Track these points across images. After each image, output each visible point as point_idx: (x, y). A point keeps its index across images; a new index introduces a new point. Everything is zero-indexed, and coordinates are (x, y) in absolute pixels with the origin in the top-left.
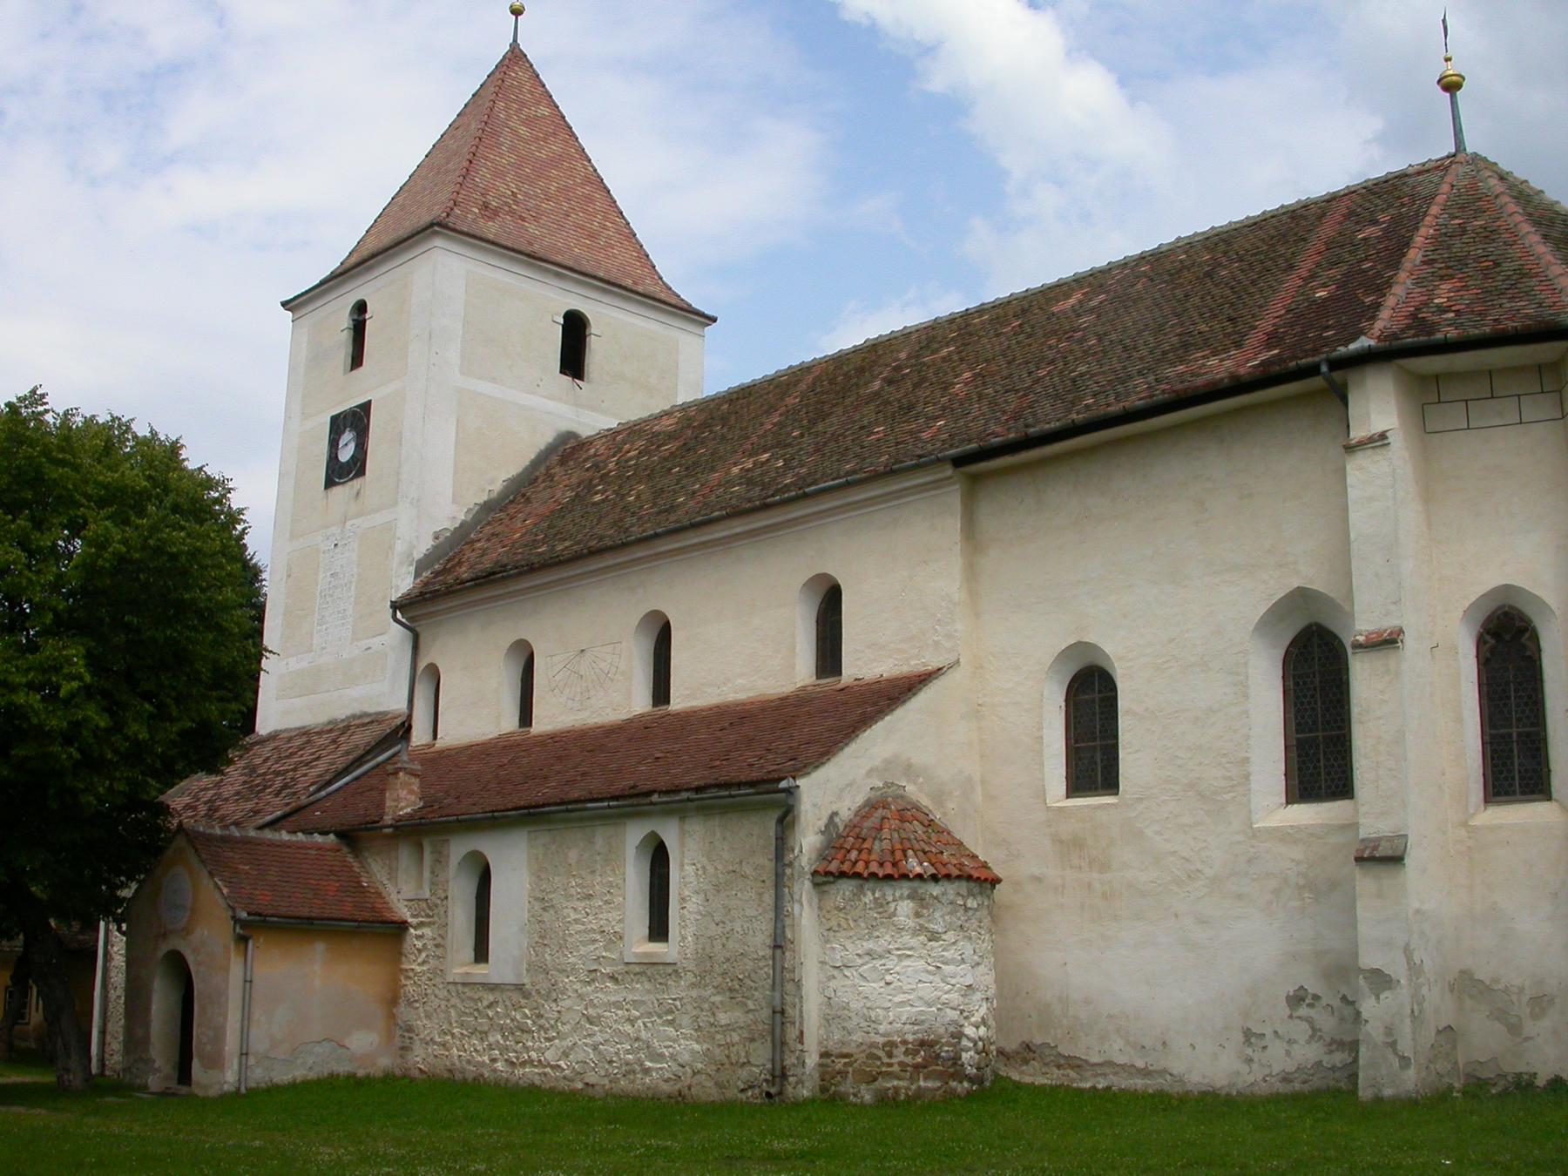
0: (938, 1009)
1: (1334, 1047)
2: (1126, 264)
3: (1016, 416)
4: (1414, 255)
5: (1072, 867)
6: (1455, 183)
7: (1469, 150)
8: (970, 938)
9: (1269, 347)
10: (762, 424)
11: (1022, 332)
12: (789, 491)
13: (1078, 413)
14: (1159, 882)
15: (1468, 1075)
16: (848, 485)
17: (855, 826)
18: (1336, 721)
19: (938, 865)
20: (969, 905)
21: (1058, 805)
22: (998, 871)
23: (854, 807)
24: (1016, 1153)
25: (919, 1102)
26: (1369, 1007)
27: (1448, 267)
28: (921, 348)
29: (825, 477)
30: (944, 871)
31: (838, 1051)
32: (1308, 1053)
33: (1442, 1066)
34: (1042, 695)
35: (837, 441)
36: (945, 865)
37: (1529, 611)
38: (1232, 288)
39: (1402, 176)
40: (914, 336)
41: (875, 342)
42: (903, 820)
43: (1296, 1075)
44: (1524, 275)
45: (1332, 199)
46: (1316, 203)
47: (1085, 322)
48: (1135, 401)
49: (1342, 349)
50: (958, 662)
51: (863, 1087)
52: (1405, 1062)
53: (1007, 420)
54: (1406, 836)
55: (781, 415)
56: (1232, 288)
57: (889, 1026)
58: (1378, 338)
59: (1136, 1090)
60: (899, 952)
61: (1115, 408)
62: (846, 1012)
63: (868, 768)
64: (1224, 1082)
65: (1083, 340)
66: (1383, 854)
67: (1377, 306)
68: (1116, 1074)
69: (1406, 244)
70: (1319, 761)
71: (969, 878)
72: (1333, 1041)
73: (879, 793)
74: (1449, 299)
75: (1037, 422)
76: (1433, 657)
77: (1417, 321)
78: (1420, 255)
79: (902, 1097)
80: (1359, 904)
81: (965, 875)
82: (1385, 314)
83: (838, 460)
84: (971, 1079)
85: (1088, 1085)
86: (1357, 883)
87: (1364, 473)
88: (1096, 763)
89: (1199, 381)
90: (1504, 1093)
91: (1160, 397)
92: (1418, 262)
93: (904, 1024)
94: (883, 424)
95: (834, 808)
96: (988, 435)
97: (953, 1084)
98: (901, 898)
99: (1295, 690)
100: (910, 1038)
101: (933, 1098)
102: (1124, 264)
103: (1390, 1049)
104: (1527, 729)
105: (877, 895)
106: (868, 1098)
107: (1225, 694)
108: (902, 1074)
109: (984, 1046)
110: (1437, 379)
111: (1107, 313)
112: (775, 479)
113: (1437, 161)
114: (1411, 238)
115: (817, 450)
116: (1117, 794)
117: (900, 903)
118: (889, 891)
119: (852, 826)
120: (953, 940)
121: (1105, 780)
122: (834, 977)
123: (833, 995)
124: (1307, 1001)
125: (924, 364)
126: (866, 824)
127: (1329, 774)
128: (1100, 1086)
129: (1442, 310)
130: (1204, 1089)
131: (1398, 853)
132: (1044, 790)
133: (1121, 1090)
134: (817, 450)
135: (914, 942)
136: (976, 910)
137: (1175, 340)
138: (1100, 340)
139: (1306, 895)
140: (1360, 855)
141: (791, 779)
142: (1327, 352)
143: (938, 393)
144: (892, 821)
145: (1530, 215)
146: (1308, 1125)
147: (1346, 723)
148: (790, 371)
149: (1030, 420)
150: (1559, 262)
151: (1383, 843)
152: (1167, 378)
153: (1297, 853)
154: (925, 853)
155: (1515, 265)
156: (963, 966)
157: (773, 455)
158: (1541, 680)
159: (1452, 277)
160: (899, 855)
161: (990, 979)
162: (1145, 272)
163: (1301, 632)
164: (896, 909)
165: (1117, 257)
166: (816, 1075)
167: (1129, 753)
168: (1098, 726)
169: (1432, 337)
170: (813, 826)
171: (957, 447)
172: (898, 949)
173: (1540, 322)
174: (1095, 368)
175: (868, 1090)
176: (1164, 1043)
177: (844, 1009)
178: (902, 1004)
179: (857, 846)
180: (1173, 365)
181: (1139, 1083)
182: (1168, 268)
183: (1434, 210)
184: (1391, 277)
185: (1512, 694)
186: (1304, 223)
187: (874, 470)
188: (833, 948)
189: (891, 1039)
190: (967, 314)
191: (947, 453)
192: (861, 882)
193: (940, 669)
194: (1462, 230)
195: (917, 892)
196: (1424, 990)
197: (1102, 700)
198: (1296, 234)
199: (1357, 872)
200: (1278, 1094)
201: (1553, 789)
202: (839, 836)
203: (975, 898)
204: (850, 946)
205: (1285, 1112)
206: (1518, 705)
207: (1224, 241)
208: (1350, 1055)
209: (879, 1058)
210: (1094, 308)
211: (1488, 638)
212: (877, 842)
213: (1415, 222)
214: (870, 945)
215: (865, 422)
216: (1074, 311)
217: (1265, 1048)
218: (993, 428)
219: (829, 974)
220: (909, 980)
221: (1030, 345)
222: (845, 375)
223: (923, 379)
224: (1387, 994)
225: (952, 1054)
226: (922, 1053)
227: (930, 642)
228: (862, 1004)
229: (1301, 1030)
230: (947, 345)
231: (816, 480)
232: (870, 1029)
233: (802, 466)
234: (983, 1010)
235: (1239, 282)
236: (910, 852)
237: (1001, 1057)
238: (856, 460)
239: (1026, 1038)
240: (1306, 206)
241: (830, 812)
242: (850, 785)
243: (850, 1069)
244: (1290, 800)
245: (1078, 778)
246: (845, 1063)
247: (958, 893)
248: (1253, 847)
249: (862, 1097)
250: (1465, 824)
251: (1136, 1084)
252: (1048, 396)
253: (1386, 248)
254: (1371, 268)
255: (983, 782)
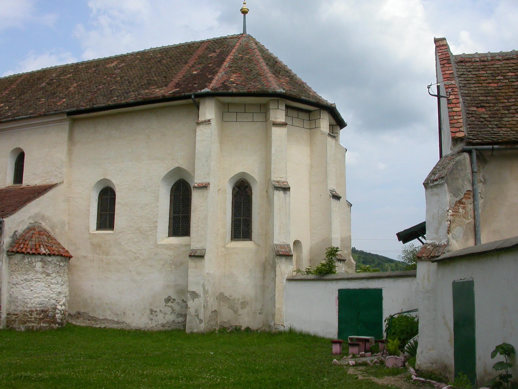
0: (49, 300)
1: (179, 316)
2: (133, 54)
3: (90, 100)
4: (226, 64)
5: (96, 253)
6: (241, 43)
7: (247, 33)
8: (61, 276)
9: (176, 87)
10: (2, 94)
11: (96, 73)
12: (9, 118)
13: (111, 102)
14: (125, 260)
15: (221, 326)
16: (30, 118)
17: (23, 236)
18: (186, 211)
19: (51, 251)
20: (61, 265)
21: (94, 232)
22: (71, 253)
23: (23, 229)
24: (72, 348)
25: (41, 331)
26: (190, 303)
27: (236, 69)
28: (61, 74)
29: (22, 114)
30: (53, 253)
31: (13, 313)
32: (171, 318)
33: (213, 323)
34: (91, 195)
35: (28, 102)
36: (53, 251)
37: (250, 181)
38: (166, 67)
39: (225, 38)
40: (58, 70)
41: (45, 70)
42: (40, 235)
43: (166, 325)
44: (259, 75)
45: (202, 42)
46: (197, 43)
47: (117, 72)
48: (131, 100)
49: (199, 91)
50: (63, 182)
51: (21, 325)
52: (201, 321)
53: (87, 102)
54: (205, 249)
55: (9, 91)
56: (166, 67)
57: (31, 305)
58: (211, 89)
59: (114, 328)
60: (36, 280)
61: (123, 102)
62: (16, 300)
63: (29, 216)
64: (143, 326)
65: (116, 78)
66: (198, 255)
67: (212, 79)
68: (108, 323)
69: (224, 60)
70: (180, 223)
71: (61, 255)
72: (179, 314)
73: (32, 225)
74: (235, 79)
75: (97, 103)
76: (218, 193)
77: (224, 85)
78: (228, 64)
79: (35, 329)
80: (189, 270)
81: (60, 254)
82: (214, 82)
83: (28, 109)
84: (59, 324)
85: (98, 326)
86: (189, 264)
87: (202, 132)
88: (107, 219)
89: (152, 96)
90: (232, 332)
91: (139, 100)
92: (226, 67)
93: (36, 304)
94: (45, 98)
95: (16, 229)
96: (80, 106)
97: (53, 325)
98: (38, 261)
99: (174, 200)
100: (38, 309)
101: (46, 330)
102: (132, 54)
103: (197, 317)
104: (246, 218)
105: (29, 260)
106: (23, 329)
107: (151, 199)
108: (35, 321)
109: (64, 312)
110: (228, 105)
111: (124, 70)
112: (4, 113)
113: (237, 35)
114: (225, 59)
115: (20, 105)
116: (113, 230)
117: (37, 263)
118: (33, 259)
119: (22, 236)
120: (55, 276)
121: (110, 225)
122: (13, 287)
123: (12, 294)
124: (171, 301)
125: (61, 79)
126: (27, 235)
127: (183, 228)
128: (102, 327)
129: (232, 83)
130: (136, 328)
131: (203, 255)
132: (89, 227)
133: (109, 328)
134: (20, 105)
135: (41, 276)
136: (63, 266)
137: (146, 81)
138: (121, 78)
139: (173, 267)
140: (190, 255)
141: (1, 218)
142: (194, 92)
143: (65, 90)
144: (36, 235)
145: (263, 56)
146: (169, 341)
147: (189, 212)
148: (14, 76)
149: (95, 103)
150: (270, 72)
151: (198, 251)
152: (142, 94)
153: (171, 253)
154: (47, 246)
155: (257, 72)
156: (58, 285)
157: (5, 104)
158: (251, 203)
159: (237, 73)
160: (38, 246)
161: (67, 290)
162: (138, 58)
163: (176, 182)
164: (35, 265)
165: (130, 52)
166: (5, 321)
167: (118, 217)
168: (108, 207)
169: (228, 91)
170: (8, 235)
171: (69, 109)
172: (36, 279)
173: (262, 90)
174: (118, 88)
175: (23, 327)
176: (124, 313)
177: (16, 298)
178: (36, 297)
179: (23, 243)
180: (144, 89)
181: (115, 326)
182: (147, 57)
183: (234, 50)
184: (218, 70)
185: (242, 207)
186: (192, 49)
187: (40, 114)
188: (13, 278)
189: (31, 309)
190: (77, 64)
191: (65, 110)
192: (24, 255)
193: (56, 184)
194: (242, 58)
195: (43, 260)
196: (208, 299)
197: (110, 198)
198: (189, 52)
199: (190, 260)
200: (160, 331)
201: (252, 237)
202: (17, 239)
203: (63, 262)
204: (19, 277)
205: (162, 336)
206: (243, 210)
207: (166, 51)
208: (184, 319)
209: (27, 316)
210: (120, 67)
211: (236, 188)
212: (30, 242)
213: (228, 52)
214: (26, 277)
215: (38, 97)
216: (114, 68)
217: (157, 315)
218: (82, 104)
219: (11, 286)
220: (39, 289)
221: (98, 77)
222: (33, 80)
223: (60, 84)
224: (197, 299)
225: (52, 315)
226: (42, 314)
227: (54, 175)
228: (22, 297)
229: (169, 310)
230: (70, 74)
231: (19, 115)
232: (25, 306)
233: (15, 110)
234: (64, 300)
235: (169, 65)
236: (42, 246)
237: (69, 316)
238: (34, 110)
239: (78, 310)
240: (194, 43)
241: (14, 230)
242: (22, 221)
243: (17, 319)
244: (169, 236)
245: (100, 224)
246: (15, 317)
247: (57, 261)
248: (157, 250)
249: (21, 329)
250: (224, 247)
251: (114, 326)
252: (102, 95)
253: (217, 61)
254: (212, 66)
255: (68, 223)
